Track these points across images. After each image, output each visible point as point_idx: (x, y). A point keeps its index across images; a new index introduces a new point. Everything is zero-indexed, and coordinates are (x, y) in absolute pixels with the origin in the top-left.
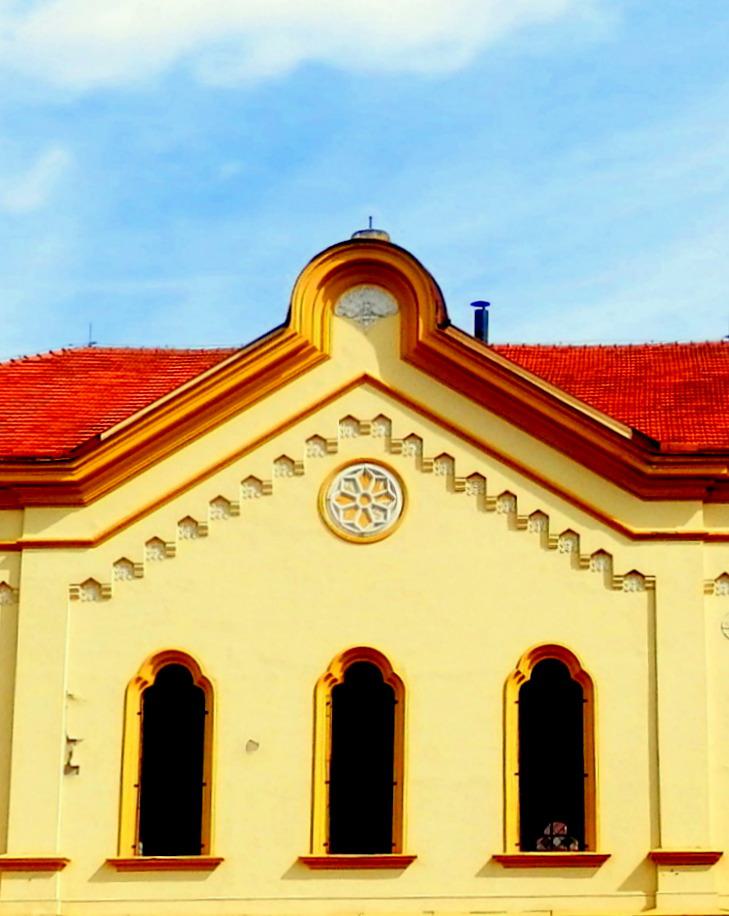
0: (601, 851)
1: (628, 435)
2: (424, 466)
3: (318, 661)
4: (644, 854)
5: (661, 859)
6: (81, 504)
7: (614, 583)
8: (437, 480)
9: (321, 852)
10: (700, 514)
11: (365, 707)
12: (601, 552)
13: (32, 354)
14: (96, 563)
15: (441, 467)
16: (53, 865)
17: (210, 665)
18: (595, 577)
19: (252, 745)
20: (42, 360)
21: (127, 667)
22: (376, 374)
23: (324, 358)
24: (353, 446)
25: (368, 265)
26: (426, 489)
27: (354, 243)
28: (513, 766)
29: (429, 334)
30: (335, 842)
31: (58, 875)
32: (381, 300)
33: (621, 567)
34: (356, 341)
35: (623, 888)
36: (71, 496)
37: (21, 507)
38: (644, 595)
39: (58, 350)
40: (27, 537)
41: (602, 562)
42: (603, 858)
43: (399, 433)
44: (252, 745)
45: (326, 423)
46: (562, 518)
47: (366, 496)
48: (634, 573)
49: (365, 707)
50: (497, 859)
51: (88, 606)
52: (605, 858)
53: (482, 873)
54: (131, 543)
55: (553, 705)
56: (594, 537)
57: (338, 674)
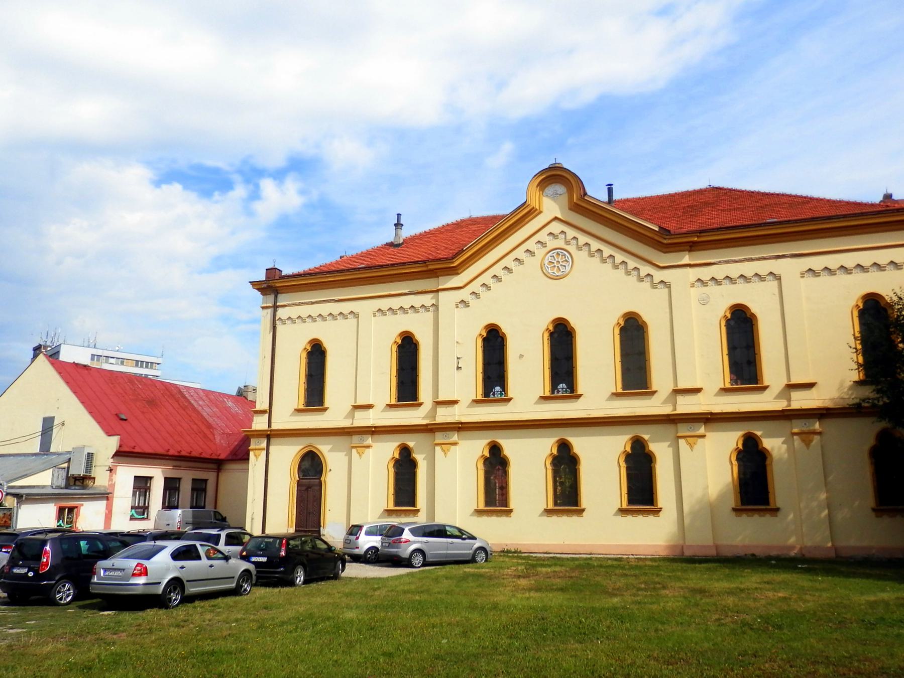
0: (579, 393)
1: (657, 229)
2: (579, 248)
3: (544, 322)
4: (783, 385)
5: (678, 392)
6: (458, 274)
7: (654, 286)
8: (584, 253)
9: (394, 402)
10: (687, 257)
11: (562, 338)
12: (648, 275)
13: (450, 222)
14: (464, 294)
15: (586, 248)
16: (455, 402)
17: (505, 328)
18: (646, 284)
19: (521, 356)
20: (453, 224)
21: (478, 330)
22: (560, 216)
23: (541, 212)
24: (552, 243)
25: (555, 176)
26: (580, 256)
27: (549, 169)
28: (618, 359)
29: (578, 199)
30: (399, 399)
31: (814, 390)
32: (560, 189)
33: (657, 279)
34: (551, 206)
35: (663, 403)
36: (454, 271)
37: (438, 277)
38: (667, 290)
39: (459, 220)
40: (440, 287)
41: (649, 279)
42: (655, 392)
43: (569, 237)
44: (521, 356)
45: (543, 236)
46: (632, 263)
47: (558, 262)
48: (662, 281)
49: (562, 338)
50: (613, 394)
51: (462, 310)
53: (716, 395)
54: (475, 286)
55: (633, 332)
56: (645, 269)
57: (551, 328)
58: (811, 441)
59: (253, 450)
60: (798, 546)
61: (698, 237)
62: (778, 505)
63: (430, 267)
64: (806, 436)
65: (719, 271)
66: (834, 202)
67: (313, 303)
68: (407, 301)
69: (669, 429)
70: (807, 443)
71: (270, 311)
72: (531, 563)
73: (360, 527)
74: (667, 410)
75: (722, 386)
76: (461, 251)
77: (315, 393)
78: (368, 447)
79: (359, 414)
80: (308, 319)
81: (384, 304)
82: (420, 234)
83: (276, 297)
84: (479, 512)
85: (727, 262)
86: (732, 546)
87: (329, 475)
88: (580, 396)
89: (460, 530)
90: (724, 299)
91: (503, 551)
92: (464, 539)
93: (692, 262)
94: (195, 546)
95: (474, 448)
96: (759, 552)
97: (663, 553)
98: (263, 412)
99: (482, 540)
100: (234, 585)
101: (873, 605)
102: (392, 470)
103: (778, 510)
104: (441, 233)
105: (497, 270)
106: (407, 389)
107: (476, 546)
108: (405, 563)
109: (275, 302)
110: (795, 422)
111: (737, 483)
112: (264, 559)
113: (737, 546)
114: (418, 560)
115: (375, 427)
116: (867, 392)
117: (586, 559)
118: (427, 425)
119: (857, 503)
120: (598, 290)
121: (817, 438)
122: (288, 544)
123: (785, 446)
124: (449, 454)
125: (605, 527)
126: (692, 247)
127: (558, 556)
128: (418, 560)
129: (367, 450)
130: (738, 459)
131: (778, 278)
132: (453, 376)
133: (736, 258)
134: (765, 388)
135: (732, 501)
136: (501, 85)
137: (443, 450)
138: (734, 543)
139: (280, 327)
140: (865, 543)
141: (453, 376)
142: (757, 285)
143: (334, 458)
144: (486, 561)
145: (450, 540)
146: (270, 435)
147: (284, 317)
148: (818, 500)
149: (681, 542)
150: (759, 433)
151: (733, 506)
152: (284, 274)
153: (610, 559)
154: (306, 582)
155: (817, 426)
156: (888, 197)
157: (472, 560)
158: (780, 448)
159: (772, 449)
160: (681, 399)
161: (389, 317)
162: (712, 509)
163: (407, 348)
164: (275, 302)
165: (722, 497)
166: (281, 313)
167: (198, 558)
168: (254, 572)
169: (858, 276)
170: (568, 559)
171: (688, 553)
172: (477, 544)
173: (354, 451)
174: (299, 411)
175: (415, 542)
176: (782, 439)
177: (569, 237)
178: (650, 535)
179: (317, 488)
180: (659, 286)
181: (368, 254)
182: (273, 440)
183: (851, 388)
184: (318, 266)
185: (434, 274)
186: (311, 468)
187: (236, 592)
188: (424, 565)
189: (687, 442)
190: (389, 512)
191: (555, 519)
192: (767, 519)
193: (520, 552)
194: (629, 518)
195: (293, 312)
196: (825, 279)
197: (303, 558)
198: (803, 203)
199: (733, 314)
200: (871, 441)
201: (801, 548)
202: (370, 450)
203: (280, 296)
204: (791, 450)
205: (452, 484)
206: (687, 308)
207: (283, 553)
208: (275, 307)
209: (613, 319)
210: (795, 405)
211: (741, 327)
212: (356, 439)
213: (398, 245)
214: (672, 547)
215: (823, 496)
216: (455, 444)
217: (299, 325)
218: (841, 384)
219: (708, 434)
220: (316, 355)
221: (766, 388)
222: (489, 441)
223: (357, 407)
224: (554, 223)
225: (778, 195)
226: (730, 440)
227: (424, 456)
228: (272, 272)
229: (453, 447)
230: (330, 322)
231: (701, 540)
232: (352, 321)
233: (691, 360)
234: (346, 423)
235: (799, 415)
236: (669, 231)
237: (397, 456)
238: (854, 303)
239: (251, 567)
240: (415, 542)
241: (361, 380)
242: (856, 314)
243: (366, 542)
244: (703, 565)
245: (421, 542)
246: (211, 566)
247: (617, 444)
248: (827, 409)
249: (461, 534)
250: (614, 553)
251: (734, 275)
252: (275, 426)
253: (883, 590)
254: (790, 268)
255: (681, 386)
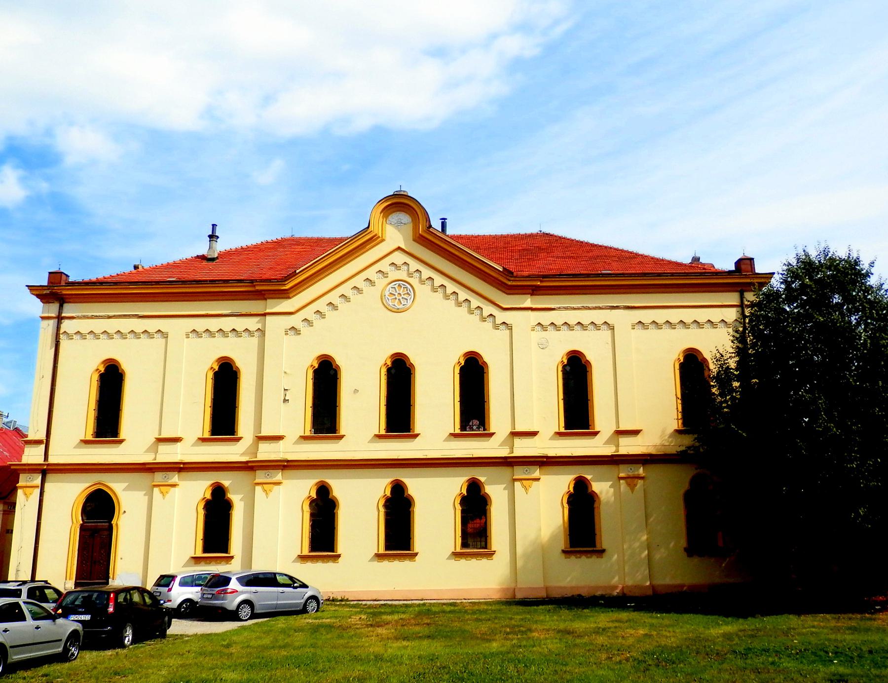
0: (492, 431)
2: (422, 282)
3: (382, 358)
6: (289, 298)
7: (496, 327)
8: (427, 287)
11: (400, 376)
14: (295, 321)
16: (279, 438)
18: (488, 325)
19: (356, 391)
21: (308, 361)
22: (403, 247)
24: (394, 275)
25: (400, 204)
26: (423, 291)
27: (394, 196)
28: (458, 398)
32: (405, 218)
33: (499, 321)
34: (395, 234)
36: (285, 294)
37: (266, 299)
38: (610, 331)
40: (268, 311)
41: (491, 319)
43: (412, 269)
45: (384, 265)
46: (475, 302)
49: (400, 376)
50: (302, 437)
51: (292, 336)
52: (493, 434)
54: (308, 313)
55: (473, 375)
56: (488, 309)
57: (389, 363)
58: (635, 485)
59: (21, 487)
60: (621, 586)
61: (541, 281)
62: (604, 547)
63: (258, 288)
64: (631, 480)
65: (558, 317)
66: (657, 259)
67: (109, 317)
68: (227, 324)
69: (505, 471)
70: (632, 487)
71: (52, 323)
72: (377, 612)
73: (173, 578)
74: (504, 452)
75: (377, 433)
76: (294, 274)
77: (107, 424)
78: (174, 486)
79: (163, 448)
80: (94, 338)
81: (200, 324)
82: (236, 250)
83: (61, 306)
84: (303, 558)
85: (566, 309)
86: (561, 588)
87: (122, 517)
88: (417, 435)
89: (291, 578)
90: (561, 345)
91: (328, 600)
92: (296, 588)
93: (534, 306)
94: (17, 605)
95: (298, 491)
96: (585, 593)
97: (496, 596)
98: (38, 442)
99: (314, 588)
100: (60, 649)
101: (728, 637)
102: (202, 513)
103: (603, 551)
104: (260, 250)
105: (333, 297)
106: (223, 421)
107: (307, 596)
108: (233, 616)
109: (60, 312)
110: (622, 467)
111: (567, 525)
112: (87, 617)
113: (565, 588)
114: (246, 611)
115: (184, 463)
116: (687, 440)
117: (419, 605)
118: (247, 462)
119: (672, 545)
120: (440, 327)
121: (640, 482)
122: (116, 598)
123: (612, 490)
124: (271, 495)
125: (437, 570)
126: (534, 291)
127: (394, 603)
128: (246, 611)
129: (172, 489)
130: (569, 502)
131: (612, 328)
132: (276, 409)
133: (111, 314)
134: (596, 433)
135: (562, 543)
136: (268, 99)
137: (265, 491)
138: (562, 584)
139: (64, 343)
140: (678, 581)
141: (276, 409)
142: (592, 333)
143: (128, 496)
144: (317, 611)
145: (281, 589)
146: (45, 471)
147: (71, 331)
148: (640, 543)
149: (513, 585)
150: (589, 477)
151: (563, 548)
152: (71, 279)
153: (444, 604)
154: (134, 642)
155: (641, 471)
156: (696, 259)
157: (304, 610)
158: (607, 492)
159: (601, 493)
160: (518, 441)
161: (206, 340)
162: (543, 551)
163: (226, 378)
164: (60, 312)
165: (553, 538)
166: (66, 325)
167: (22, 618)
168: (82, 633)
169: (680, 331)
170: (401, 606)
171: (519, 596)
172: (309, 593)
173: (156, 490)
174: (86, 442)
175: (243, 593)
176: (611, 483)
177: (412, 269)
178: (483, 579)
179: (106, 533)
180: (692, 326)
181: (175, 266)
182: (49, 477)
183: (671, 436)
184: (114, 274)
185: (261, 295)
186: (99, 511)
187: (63, 657)
188: (251, 618)
189: (522, 484)
190: (197, 560)
191: (386, 564)
192: (594, 560)
193: (347, 600)
194: (463, 562)
195: (84, 326)
196: (653, 332)
197: (118, 617)
198: (630, 258)
199: (569, 360)
200: (686, 486)
201: (623, 588)
202: (176, 489)
203: (67, 306)
204: (618, 493)
205: (270, 529)
206: (526, 349)
207: (111, 610)
208: (60, 319)
209: (454, 359)
210: (623, 451)
211: (576, 374)
212: (159, 477)
213: (213, 259)
214: (504, 590)
215: (645, 538)
216: (279, 483)
217: (90, 341)
218: (663, 432)
219: (543, 478)
220: (111, 381)
221: (492, 435)
222: (317, 480)
223: (160, 440)
224: (396, 253)
225: (606, 247)
226: (560, 484)
227: (241, 496)
228: (56, 277)
229: (276, 487)
230: (131, 341)
231: (533, 582)
232: (159, 341)
233: (526, 402)
234: (148, 458)
235: (211, 468)
236: (512, 273)
237: (208, 496)
238: (676, 357)
239: (79, 627)
240: (243, 593)
241: (166, 408)
242: (677, 366)
243: (178, 594)
244: (541, 607)
245: (250, 592)
246: (37, 628)
247: (454, 485)
248: (650, 455)
249: (293, 582)
250: (446, 597)
251: (674, 320)
252: (52, 460)
253: (727, 624)
254: (622, 319)
255: (519, 429)
